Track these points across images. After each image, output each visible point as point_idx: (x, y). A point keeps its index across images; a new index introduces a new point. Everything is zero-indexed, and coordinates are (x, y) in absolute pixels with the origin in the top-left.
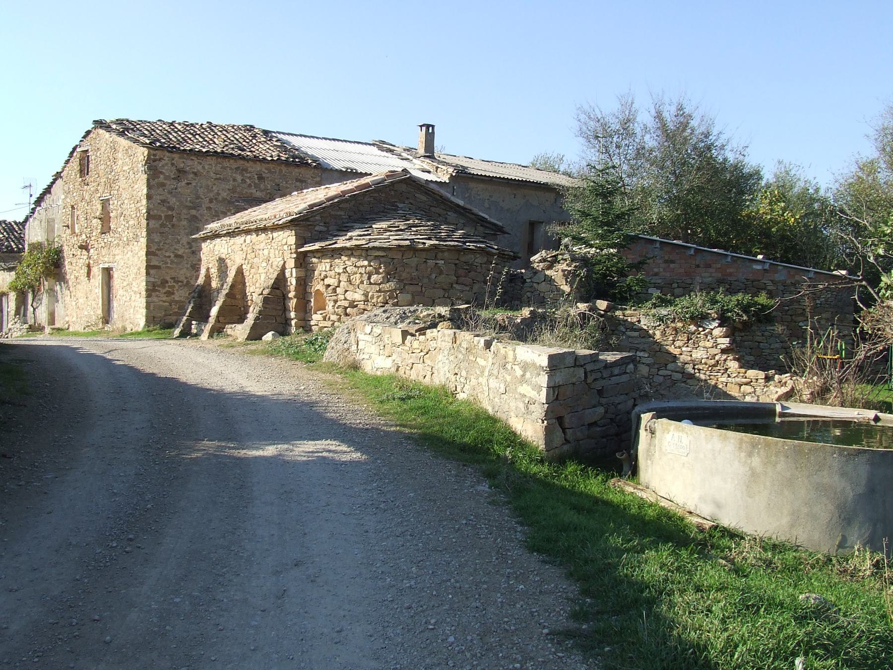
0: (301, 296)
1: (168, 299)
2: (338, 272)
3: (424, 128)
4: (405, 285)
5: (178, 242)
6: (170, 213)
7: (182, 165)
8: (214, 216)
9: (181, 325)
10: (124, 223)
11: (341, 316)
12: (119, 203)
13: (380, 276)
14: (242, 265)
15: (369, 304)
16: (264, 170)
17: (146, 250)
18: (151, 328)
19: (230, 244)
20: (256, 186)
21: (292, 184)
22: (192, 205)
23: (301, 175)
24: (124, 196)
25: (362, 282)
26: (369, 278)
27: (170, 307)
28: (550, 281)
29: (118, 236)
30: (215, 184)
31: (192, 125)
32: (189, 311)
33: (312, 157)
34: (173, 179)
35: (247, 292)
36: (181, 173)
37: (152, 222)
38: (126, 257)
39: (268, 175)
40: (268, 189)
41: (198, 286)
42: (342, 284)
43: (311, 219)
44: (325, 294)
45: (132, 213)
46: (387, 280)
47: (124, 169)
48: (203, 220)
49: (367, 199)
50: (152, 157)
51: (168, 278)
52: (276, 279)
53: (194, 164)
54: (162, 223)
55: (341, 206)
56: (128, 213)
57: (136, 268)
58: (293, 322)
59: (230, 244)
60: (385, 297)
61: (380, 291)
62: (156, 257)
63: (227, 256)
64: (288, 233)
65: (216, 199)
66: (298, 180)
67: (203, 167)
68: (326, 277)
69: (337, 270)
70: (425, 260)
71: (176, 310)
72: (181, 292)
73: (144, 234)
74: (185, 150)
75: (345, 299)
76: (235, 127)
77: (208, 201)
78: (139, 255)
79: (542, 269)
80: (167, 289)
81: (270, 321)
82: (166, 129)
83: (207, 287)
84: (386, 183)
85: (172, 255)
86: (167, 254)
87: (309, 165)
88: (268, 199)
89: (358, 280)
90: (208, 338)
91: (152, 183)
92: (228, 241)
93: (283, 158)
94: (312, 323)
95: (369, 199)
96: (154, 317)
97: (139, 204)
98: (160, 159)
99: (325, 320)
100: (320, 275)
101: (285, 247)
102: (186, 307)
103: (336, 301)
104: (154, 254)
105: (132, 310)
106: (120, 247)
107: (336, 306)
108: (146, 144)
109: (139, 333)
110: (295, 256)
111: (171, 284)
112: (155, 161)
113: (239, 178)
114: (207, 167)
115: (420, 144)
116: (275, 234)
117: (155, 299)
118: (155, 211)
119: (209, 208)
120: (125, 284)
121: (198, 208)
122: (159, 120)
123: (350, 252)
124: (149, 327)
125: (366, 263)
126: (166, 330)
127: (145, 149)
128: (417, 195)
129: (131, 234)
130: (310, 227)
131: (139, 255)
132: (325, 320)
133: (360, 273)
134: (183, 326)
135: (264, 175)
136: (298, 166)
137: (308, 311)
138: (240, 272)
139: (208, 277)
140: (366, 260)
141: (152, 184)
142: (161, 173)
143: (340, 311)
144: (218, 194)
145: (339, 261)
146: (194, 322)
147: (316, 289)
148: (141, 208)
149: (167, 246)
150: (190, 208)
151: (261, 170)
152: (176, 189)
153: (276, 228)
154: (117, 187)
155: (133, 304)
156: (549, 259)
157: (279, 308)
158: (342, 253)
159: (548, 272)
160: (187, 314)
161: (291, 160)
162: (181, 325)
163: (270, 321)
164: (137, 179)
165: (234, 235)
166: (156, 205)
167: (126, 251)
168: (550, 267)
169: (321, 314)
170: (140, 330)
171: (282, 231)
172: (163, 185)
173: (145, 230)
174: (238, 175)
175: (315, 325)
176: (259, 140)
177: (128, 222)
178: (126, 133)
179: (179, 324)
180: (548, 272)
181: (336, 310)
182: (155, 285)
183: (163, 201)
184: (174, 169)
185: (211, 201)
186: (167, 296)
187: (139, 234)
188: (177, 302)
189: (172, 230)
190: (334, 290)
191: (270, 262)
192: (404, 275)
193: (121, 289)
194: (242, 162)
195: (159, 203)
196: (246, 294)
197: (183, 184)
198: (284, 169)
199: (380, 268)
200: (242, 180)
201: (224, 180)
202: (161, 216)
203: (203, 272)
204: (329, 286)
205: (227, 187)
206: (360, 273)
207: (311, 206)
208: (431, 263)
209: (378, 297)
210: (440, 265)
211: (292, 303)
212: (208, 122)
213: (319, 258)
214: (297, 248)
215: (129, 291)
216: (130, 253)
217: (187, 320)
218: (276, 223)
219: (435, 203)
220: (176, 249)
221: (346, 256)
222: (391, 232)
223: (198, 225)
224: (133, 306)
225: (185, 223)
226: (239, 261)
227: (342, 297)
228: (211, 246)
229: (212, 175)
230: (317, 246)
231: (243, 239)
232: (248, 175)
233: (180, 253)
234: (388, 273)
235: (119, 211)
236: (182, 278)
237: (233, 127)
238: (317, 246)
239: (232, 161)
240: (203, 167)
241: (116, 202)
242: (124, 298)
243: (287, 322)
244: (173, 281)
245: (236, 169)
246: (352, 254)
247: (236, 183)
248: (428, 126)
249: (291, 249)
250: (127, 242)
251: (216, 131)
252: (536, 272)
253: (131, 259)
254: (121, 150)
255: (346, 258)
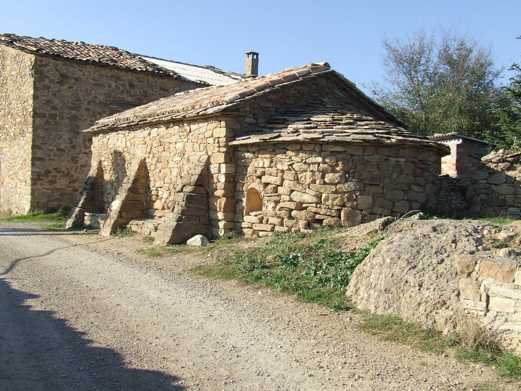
0: (231, 195)
1: (51, 187)
2: (281, 168)
3: (251, 56)
4: (365, 185)
5: (61, 137)
6: (54, 112)
7: (65, 71)
8: (92, 116)
9: (74, 215)
10: (11, 120)
11: (283, 219)
12: (7, 103)
13: (337, 175)
14: (145, 159)
15: (323, 207)
16: (134, 79)
17: (31, 144)
18: (36, 213)
19: (128, 138)
20: (128, 92)
21: (157, 91)
22: (72, 106)
23: (164, 85)
24: (12, 97)
25: (314, 182)
26: (323, 177)
27: (52, 194)
28: (513, 183)
29: (6, 131)
30: (93, 89)
31: (69, 43)
32: (81, 202)
33: (173, 72)
34: (57, 82)
35: (151, 186)
36: (64, 77)
37: (38, 120)
38: (12, 150)
39: (138, 83)
40: (137, 95)
41: (90, 178)
42: (286, 183)
43: (241, 110)
44: (262, 194)
45: (19, 112)
46: (344, 179)
47: (12, 74)
48: (82, 119)
49: (292, 92)
50: (39, 63)
51: (51, 169)
52: (200, 175)
53: (75, 71)
54: (47, 120)
55: (269, 97)
56: (16, 112)
57: (22, 159)
58: (221, 224)
59: (128, 138)
60: (342, 199)
61: (336, 192)
62: (41, 150)
63: (125, 149)
64: (213, 124)
65: (94, 102)
66: (161, 89)
67: (84, 74)
68: (264, 174)
69: (279, 166)
70: (386, 157)
71: (58, 197)
72: (62, 181)
73: (30, 130)
74: (68, 58)
75: (291, 200)
76: (104, 47)
77: (87, 103)
78: (25, 148)
79: (502, 170)
80: (50, 178)
81: (194, 222)
82: (48, 43)
83: (99, 179)
84: (313, 75)
85: (55, 149)
86: (51, 148)
87: (171, 76)
88: (137, 103)
89: (308, 178)
90: (111, 234)
91: (39, 85)
92: (126, 134)
93: (150, 70)
94: (244, 225)
95: (294, 92)
96: (38, 203)
97: (26, 104)
98: (46, 65)
99: (261, 222)
100: (256, 171)
101: (210, 141)
102: (78, 198)
103: (277, 202)
104: (39, 147)
105: (17, 196)
106: (7, 142)
107: (278, 207)
108: (34, 51)
109: (25, 218)
110: (225, 149)
111: (54, 173)
112: (41, 66)
113: (114, 85)
114: (86, 74)
115: (247, 68)
116: (194, 127)
117: (40, 187)
118: (41, 110)
119: (87, 110)
120: (11, 173)
121: (78, 109)
122: (41, 38)
123: (298, 147)
124: (34, 211)
125: (319, 159)
126: (49, 214)
127: (32, 55)
128: (335, 91)
129: (18, 130)
130: (240, 118)
131: (25, 148)
132: (261, 222)
133: (312, 171)
134: (76, 217)
135: (134, 83)
136: (162, 77)
137: (238, 211)
138: (143, 166)
139: (100, 170)
140: (320, 155)
141: (38, 86)
142: (47, 77)
143: (283, 213)
144: (96, 97)
145: (283, 157)
146: (86, 214)
147: (250, 187)
148: (27, 107)
149: (51, 141)
150: (71, 109)
151: (132, 79)
152: (59, 91)
153: (205, 118)
154: (5, 90)
155: (19, 191)
156: (509, 159)
157: (202, 207)
158: (287, 148)
159: (510, 173)
160: (80, 205)
161: (157, 72)
162: (74, 215)
163: (194, 222)
164: (24, 82)
165: (135, 129)
166: (42, 104)
167: (12, 145)
168: (511, 168)
169: (256, 216)
170: (25, 214)
171: (205, 122)
172: (48, 87)
173: (31, 126)
174: (113, 82)
175: (248, 228)
176: (125, 57)
177: (14, 120)
178: (14, 43)
179: (71, 215)
180: (510, 173)
181: (278, 212)
182: (40, 174)
183: (48, 102)
184: (58, 74)
185: (89, 103)
186: (50, 185)
187: (25, 130)
188: (59, 189)
189: (56, 127)
190: (275, 190)
191: (186, 156)
192: (365, 174)
193: (7, 177)
194: (116, 71)
195: (44, 104)
196: (150, 188)
197: (66, 87)
198: (151, 79)
199: (337, 165)
200: (116, 86)
201: (101, 85)
202: (46, 115)
203: (94, 164)
204: (266, 185)
205: (104, 92)
206: (312, 171)
207: (243, 95)
208: (393, 160)
209: (334, 199)
210: (401, 163)
211: (221, 203)
212: (81, 42)
213: (254, 153)
214: (227, 141)
215: (15, 179)
216: (16, 146)
217: (79, 211)
218: (200, 114)
219: (350, 100)
220: (58, 144)
221: (293, 151)
222: (339, 125)
223: (78, 123)
224: (19, 193)
225: (66, 121)
226: (140, 153)
227: (287, 198)
228: (104, 140)
229: (91, 81)
230: (255, 139)
231: (147, 132)
232: (121, 82)
233: (62, 147)
234: (346, 172)
235: (7, 110)
236: (63, 169)
237: (102, 46)
238: (255, 139)
239: (108, 70)
240: (84, 74)
241: (4, 103)
242: (10, 185)
243: (212, 223)
244: (55, 171)
245: (111, 76)
246: (302, 148)
247: (111, 89)
248: (254, 54)
249: (218, 142)
250: (14, 137)
251: (90, 48)
252: (492, 172)
253: (17, 151)
254: (9, 58)
255: (293, 154)
